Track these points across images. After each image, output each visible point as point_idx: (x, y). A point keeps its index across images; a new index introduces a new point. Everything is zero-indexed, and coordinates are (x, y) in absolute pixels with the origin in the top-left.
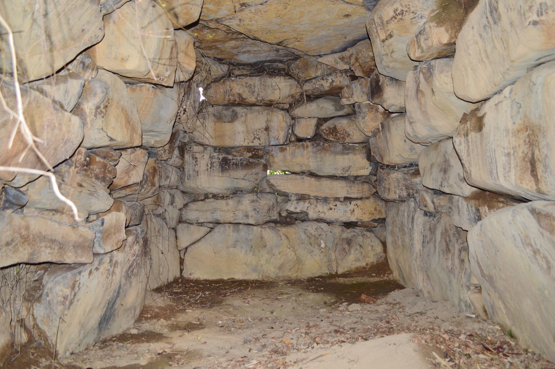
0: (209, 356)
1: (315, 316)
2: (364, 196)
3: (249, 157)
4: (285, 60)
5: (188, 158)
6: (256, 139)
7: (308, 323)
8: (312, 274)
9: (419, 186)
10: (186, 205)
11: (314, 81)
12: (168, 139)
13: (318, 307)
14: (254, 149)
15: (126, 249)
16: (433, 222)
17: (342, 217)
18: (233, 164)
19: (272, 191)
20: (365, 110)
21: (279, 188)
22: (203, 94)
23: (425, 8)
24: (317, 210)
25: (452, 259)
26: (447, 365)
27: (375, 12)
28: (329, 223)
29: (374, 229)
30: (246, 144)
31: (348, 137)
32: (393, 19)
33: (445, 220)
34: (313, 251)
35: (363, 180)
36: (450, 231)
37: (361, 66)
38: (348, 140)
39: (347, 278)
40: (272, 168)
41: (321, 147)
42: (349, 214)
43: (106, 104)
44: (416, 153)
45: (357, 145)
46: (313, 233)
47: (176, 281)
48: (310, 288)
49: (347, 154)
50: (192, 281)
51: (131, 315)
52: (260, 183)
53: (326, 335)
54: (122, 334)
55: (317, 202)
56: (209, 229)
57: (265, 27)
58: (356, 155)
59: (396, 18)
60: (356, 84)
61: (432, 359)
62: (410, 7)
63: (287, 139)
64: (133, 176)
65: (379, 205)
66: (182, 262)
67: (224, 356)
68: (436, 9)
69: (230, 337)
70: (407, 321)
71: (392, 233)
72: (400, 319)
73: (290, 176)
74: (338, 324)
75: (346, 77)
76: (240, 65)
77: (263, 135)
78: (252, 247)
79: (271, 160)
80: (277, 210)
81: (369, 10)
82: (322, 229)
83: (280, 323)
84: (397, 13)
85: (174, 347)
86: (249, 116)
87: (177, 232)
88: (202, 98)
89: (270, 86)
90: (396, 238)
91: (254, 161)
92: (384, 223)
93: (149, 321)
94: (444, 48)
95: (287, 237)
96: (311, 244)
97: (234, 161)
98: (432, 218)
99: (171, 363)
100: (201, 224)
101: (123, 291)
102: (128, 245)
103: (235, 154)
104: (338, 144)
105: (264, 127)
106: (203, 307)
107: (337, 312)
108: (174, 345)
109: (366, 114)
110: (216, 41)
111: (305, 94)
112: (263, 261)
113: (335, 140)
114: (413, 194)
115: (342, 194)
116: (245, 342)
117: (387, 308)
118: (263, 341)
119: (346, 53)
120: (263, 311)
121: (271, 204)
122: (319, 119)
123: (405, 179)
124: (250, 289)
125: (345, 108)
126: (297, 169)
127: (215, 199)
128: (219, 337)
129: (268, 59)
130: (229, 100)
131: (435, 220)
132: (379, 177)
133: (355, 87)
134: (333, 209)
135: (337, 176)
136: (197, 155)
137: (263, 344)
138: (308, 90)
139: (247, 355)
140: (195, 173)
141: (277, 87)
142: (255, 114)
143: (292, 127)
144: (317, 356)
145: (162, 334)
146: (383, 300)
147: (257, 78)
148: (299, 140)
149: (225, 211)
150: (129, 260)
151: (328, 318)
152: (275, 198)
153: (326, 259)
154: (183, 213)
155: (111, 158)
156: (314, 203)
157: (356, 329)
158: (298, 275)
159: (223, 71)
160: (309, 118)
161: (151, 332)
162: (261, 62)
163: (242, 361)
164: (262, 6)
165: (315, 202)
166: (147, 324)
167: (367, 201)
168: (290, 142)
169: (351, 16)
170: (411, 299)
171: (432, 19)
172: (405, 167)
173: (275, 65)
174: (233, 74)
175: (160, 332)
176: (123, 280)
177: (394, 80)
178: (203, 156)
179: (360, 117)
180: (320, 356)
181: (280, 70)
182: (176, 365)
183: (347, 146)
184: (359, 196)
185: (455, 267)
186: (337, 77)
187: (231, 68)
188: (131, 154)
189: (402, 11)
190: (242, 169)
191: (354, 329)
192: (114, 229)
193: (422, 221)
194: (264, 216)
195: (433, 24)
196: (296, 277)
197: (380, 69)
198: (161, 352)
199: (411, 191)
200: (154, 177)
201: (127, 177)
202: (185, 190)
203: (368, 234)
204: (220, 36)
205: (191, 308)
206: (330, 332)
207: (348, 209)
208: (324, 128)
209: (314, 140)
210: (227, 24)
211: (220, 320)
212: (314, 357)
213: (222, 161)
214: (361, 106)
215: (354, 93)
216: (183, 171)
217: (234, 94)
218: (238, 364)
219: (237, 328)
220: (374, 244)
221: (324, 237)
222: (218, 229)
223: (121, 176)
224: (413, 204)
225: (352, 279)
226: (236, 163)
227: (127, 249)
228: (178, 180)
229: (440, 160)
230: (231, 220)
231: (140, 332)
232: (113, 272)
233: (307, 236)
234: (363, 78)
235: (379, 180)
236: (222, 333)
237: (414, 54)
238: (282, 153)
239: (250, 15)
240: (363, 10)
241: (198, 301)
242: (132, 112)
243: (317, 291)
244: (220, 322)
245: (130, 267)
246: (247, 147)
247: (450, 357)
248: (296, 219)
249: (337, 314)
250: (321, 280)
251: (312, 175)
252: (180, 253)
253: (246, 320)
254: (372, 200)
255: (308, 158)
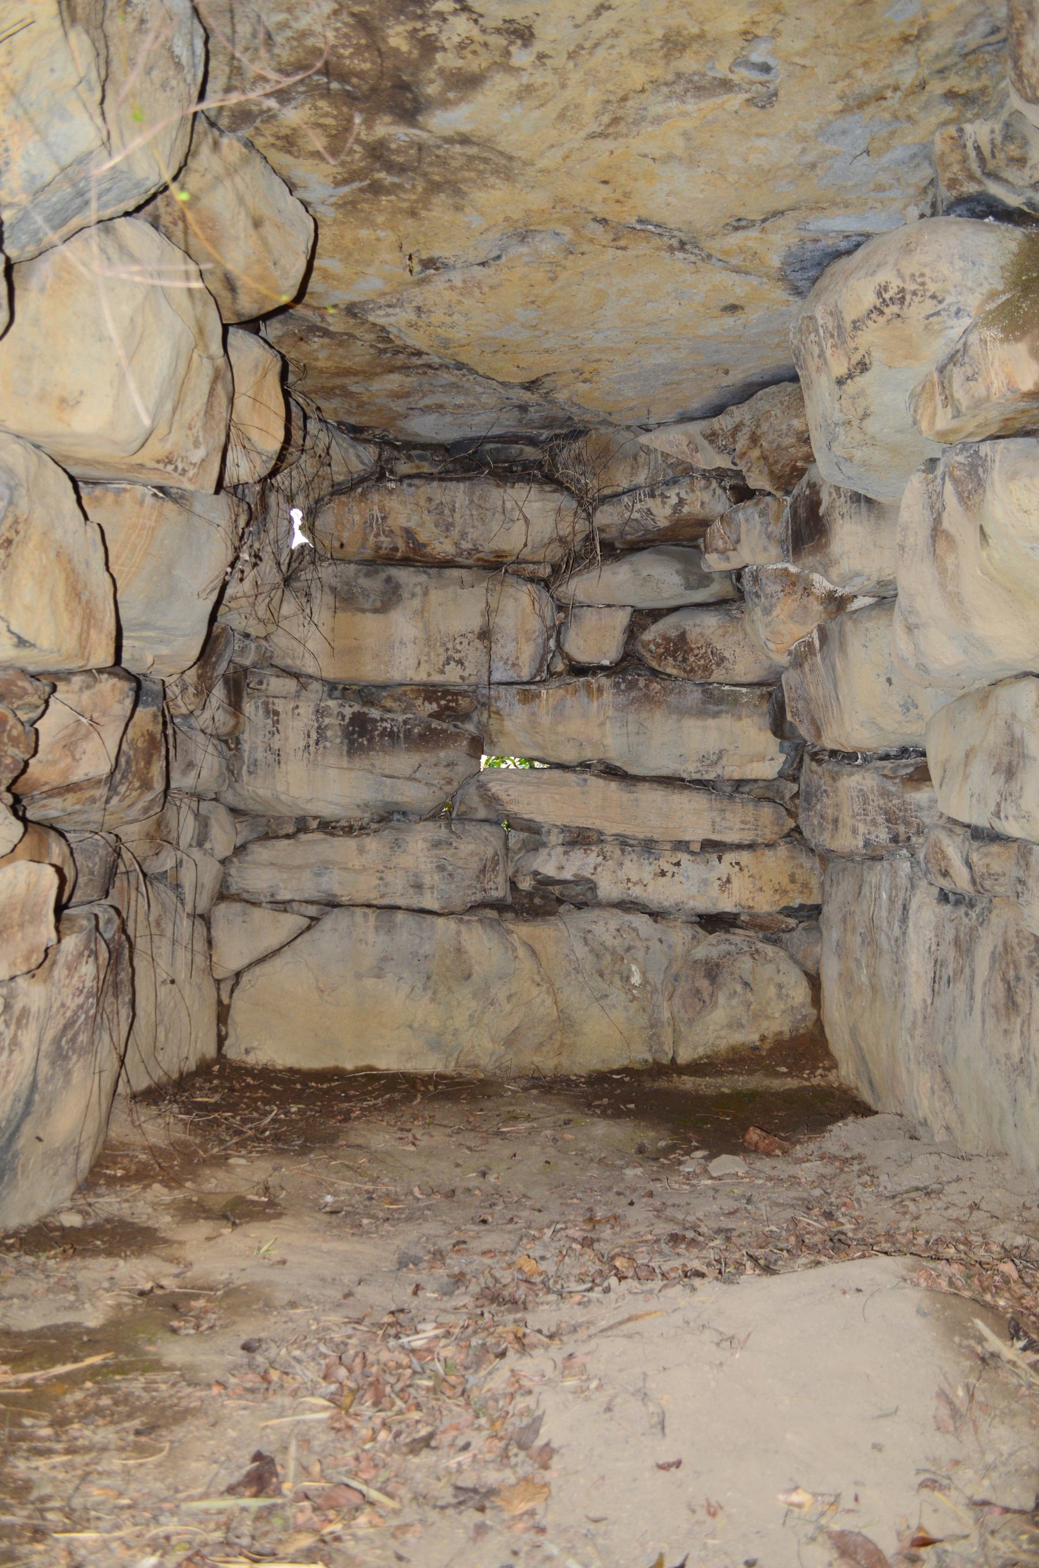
0: (293, 1305)
1: (610, 1189)
2: (760, 840)
3: (431, 715)
4: (542, 438)
5: (253, 713)
6: (452, 663)
7: (590, 1210)
8: (603, 1061)
9: (926, 813)
10: (240, 850)
11: (625, 499)
12: (195, 652)
13: (619, 1162)
14: (446, 692)
15: (56, 973)
16: (966, 920)
17: (693, 898)
18: (382, 735)
19: (493, 816)
20: (772, 588)
21: (513, 808)
22: (300, 528)
23: (969, 284)
24: (621, 875)
25: (1022, 1032)
26: (1019, 1363)
27: (818, 296)
28: (656, 915)
29: (785, 936)
30: (421, 677)
31: (718, 665)
32: (874, 316)
33: (1000, 919)
34: (606, 996)
35: (759, 792)
36: (1017, 949)
37: (765, 458)
38: (718, 675)
39: (706, 1075)
40: (497, 751)
41: (640, 694)
42: (714, 890)
43: (7, 534)
44: (920, 717)
45: (744, 690)
46: (610, 942)
47: (204, 1069)
48: (597, 1103)
49: (716, 715)
50: (250, 1071)
51: (64, 1171)
52: (460, 792)
53: (644, 1249)
54: (37, 1228)
55: (623, 851)
56: (306, 922)
57: (489, 334)
58: (740, 718)
59: (882, 313)
60: (750, 511)
61: (972, 1342)
62: (927, 280)
63: (541, 666)
64: (85, 758)
65: (802, 867)
66: (223, 1014)
67: (339, 1305)
68: (1001, 288)
69: (359, 1247)
70: (885, 1214)
71: (842, 952)
72: (864, 1206)
73: (547, 774)
74: (680, 1216)
75: (719, 491)
76: (411, 447)
77: (473, 653)
78: (429, 978)
79: (494, 725)
80: (505, 871)
81: (798, 292)
82: (635, 930)
83: (506, 1207)
84: (887, 296)
85: (189, 1274)
86: (435, 596)
87: (213, 925)
88: (299, 539)
89: (500, 509)
90: (853, 966)
91: (445, 726)
92: (817, 919)
93: (118, 1188)
94: (1022, 405)
95: (534, 952)
96: (602, 975)
97: (385, 724)
98: (963, 909)
99: (175, 1324)
100: (282, 906)
101: (43, 1100)
102: (61, 959)
103: (389, 703)
104: (689, 686)
105: (477, 630)
106: (281, 1152)
107: (677, 1178)
108: (189, 1265)
109: (774, 600)
110: (348, 372)
111: (597, 539)
112: (460, 1020)
113: (683, 674)
114: (909, 839)
115: (697, 831)
116: (405, 1262)
117: (823, 1170)
118: (456, 1263)
119: (722, 422)
120: (458, 1170)
121: (490, 852)
122: (637, 612)
123: (885, 794)
124: (418, 1100)
125: (713, 580)
126: (570, 755)
127: (326, 833)
128: (325, 1247)
129: (497, 431)
130: (378, 548)
131: (973, 915)
132: (807, 786)
133: (747, 520)
134: (669, 874)
135: (683, 780)
136: (280, 705)
137: (456, 1270)
138: (608, 526)
139: (406, 1306)
140: (271, 757)
141: (516, 514)
142: (451, 589)
143: (559, 633)
144: (619, 1319)
145: (156, 1230)
146: (812, 1146)
147: (462, 485)
148: (579, 670)
149: (355, 871)
150: (63, 1005)
151: (651, 1194)
152: (502, 835)
153: (643, 1020)
154: (233, 871)
155: (21, 698)
156: (615, 856)
157: (735, 1234)
158: (560, 1064)
159: (362, 463)
160: (609, 606)
161: (123, 1223)
162: (473, 440)
163: (391, 1325)
164: (485, 271)
165: (618, 852)
166: (112, 1199)
167: (769, 853)
168: (551, 674)
169: (742, 308)
170: (893, 1146)
171: (990, 319)
172: (886, 757)
173: (514, 449)
174: (392, 472)
175: (150, 1223)
176: (44, 1067)
177: (861, 500)
178: (297, 707)
179: (758, 610)
180: (630, 1319)
181: (526, 466)
182: (192, 1331)
183: (716, 692)
184: (747, 837)
185: (1031, 1059)
186: (693, 491)
187: (386, 454)
188: (81, 690)
189: (902, 290)
190: (408, 750)
191: (727, 1234)
192: (22, 913)
193: (933, 918)
194: (469, 887)
195: (992, 333)
196: (556, 1068)
197: (823, 470)
198: (148, 1286)
199: (902, 829)
200: (149, 763)
201: (69, 760)
202: (242, 806)
203: (769, 950)
204: (357, 359)
205: (244, 1152)
206: (657, 1241)
207: (713, 876)
208: (651, 638)
209: (621, 672)
210: (381, 321)
211: (329, 1193)
212: (612, 1322)
213: (350, 724)
214: (761, 575)
215: (743, 537)
216: (237, 749)
217: (391, 531)
218: (380, 1333)
219: (378, 1219)
220: (782, 979)
221: (640, 954)
222: (334, 922)
223: (50, 757)
224: (905, 867)
225: (719, 1080)
226: (392, 731)
227: (59, 972)
228: (221, 774)
229: (994, 738)
230: (373, 897)
231: (90, 1222)
232: (15, 1042)
233: (592, 951)
234: (769, 494)
235: (808, 793)
236: (335, 1232)
237: (932, 422)
238: (526, 707)
239: (447, 294)
240: (779, 291)
241: (267, 1133)
242: (87, 563)
243: (614, 1113)
244: (329, 1199)
245: (66, 1028)
246: (425, 685)
247: (1026, 1334)
248: (560, 901)
249: (677, 1186)
250: (627, 1079)
251: (611, 772)
252: (218, 989)
253: (406, 1195)
254: (782, 850)
255: (602, 724)
